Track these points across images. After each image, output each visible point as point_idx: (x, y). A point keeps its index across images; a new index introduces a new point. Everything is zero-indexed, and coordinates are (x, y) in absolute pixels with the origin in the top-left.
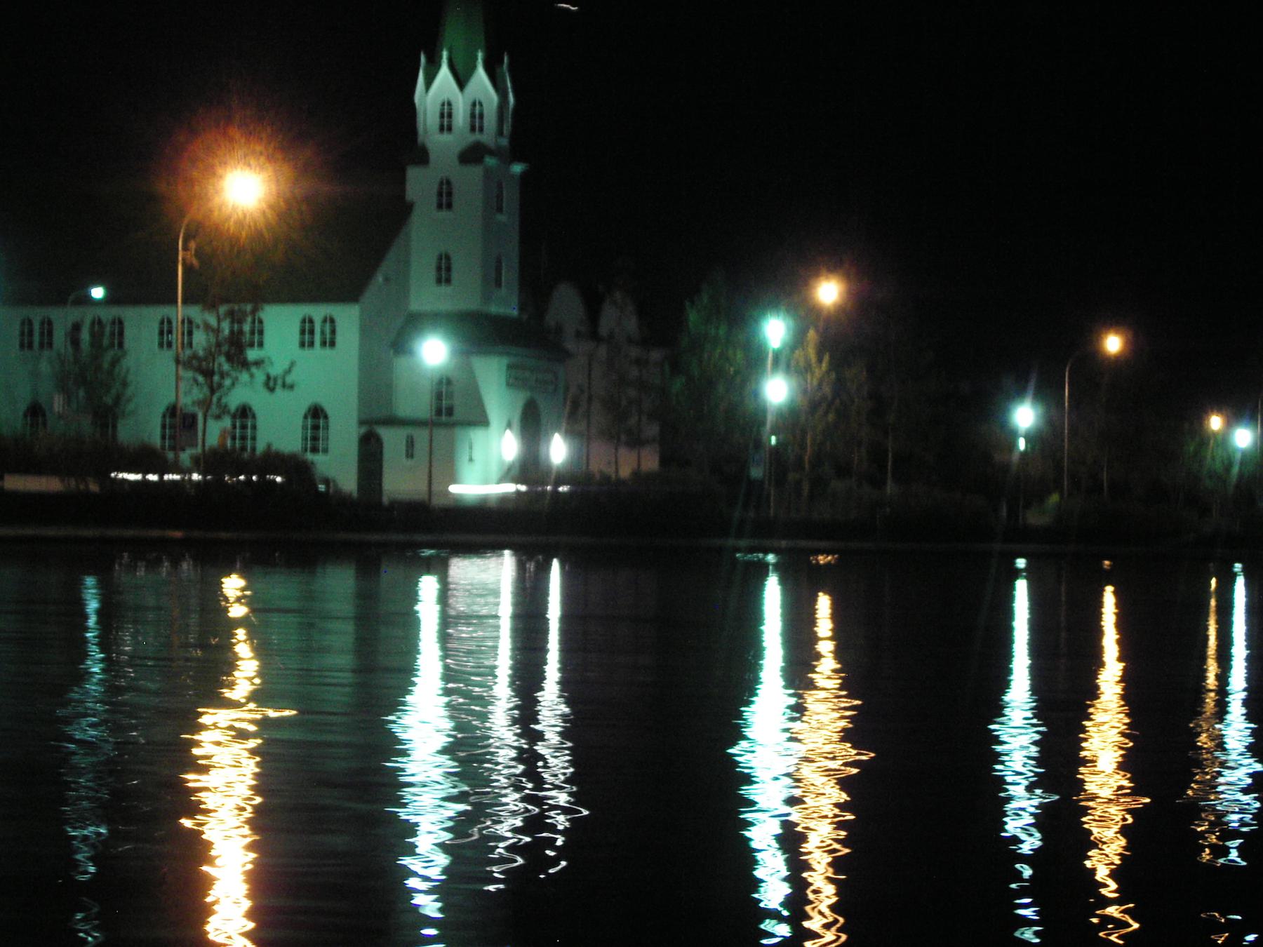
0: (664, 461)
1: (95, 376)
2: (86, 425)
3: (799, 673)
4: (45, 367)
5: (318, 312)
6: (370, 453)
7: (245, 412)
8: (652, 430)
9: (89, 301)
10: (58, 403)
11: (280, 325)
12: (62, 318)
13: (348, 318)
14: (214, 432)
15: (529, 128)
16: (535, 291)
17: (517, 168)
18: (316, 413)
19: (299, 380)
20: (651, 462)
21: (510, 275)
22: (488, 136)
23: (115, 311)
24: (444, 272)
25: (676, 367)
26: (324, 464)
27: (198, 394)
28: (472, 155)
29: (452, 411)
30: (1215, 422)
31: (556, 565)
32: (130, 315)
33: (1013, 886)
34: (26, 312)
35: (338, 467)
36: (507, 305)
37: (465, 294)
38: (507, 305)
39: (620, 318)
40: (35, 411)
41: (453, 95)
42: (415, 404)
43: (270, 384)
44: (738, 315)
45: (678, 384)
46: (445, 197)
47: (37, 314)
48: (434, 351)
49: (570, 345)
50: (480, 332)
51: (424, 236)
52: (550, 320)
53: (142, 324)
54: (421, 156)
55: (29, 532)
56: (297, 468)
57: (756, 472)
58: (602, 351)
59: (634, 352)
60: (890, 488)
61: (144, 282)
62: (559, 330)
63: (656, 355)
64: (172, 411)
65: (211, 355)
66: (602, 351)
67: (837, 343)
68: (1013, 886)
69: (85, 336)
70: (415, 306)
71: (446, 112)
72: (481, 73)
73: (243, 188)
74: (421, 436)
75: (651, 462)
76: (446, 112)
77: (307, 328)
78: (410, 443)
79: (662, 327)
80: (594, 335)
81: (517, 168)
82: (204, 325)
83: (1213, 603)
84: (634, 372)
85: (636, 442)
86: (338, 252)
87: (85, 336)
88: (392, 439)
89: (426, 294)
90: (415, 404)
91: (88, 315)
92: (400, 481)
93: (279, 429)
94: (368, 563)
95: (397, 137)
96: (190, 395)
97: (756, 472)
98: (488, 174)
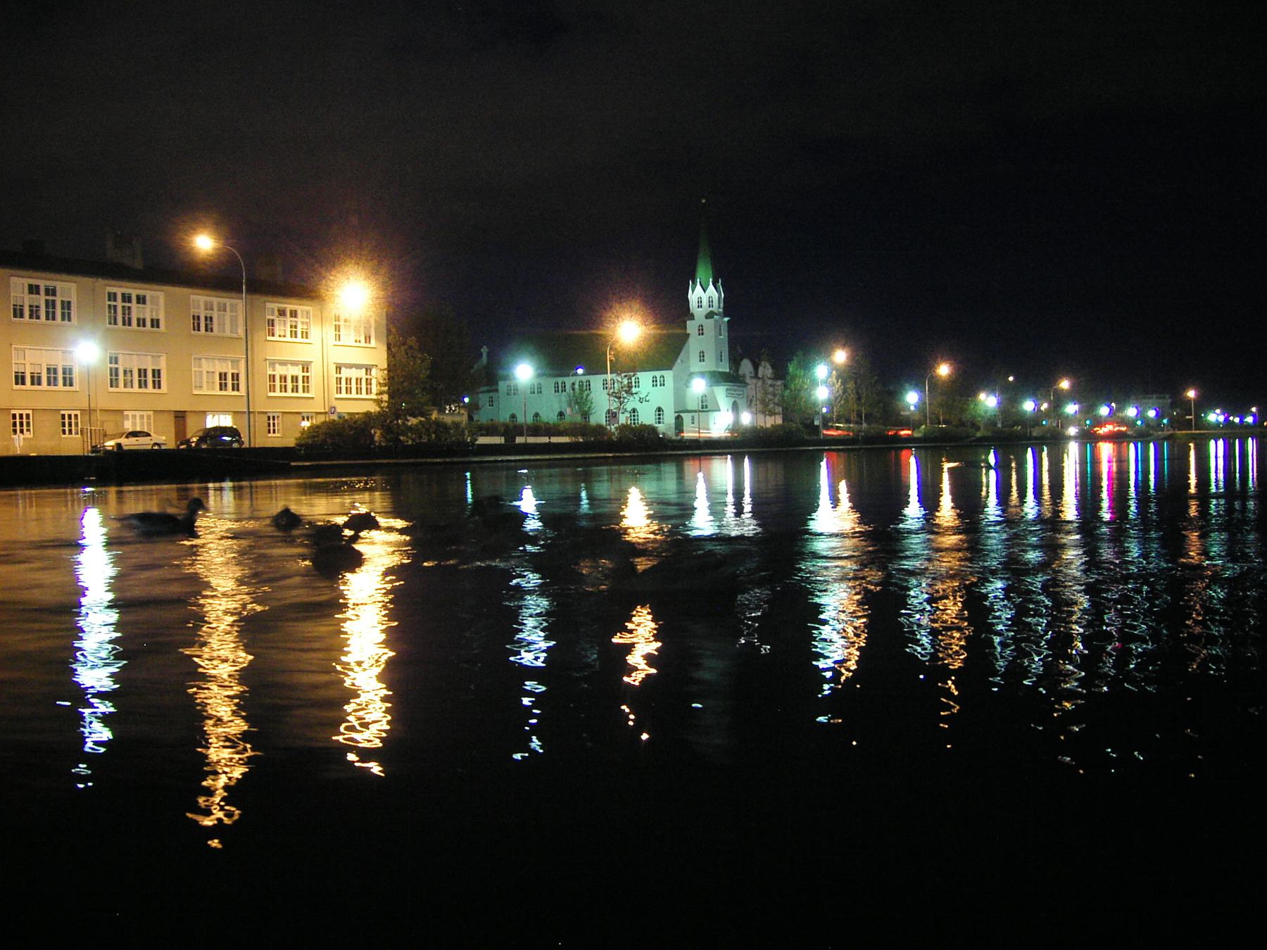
0: (784, 420)
1: (581, 400)
2: (578, 419)
3: (835, 501)
4: (564, 399)
5: (658, 374)
6: (679, 420)
7: (634, 410)
8: (779, 409)
9: (576, 374)
10: (568, 410)
11: (645, 378)
12: (568, 381)
13: (668, 375)
14: (623, 419)
15: (730, 306)
16: (735, 361)
17: (726, 319)
18: (659, 409)
19: (651, 401)
20: (779, 421)
21: (726, 355)
22: (715, 309)
23: (588, 377)
24: (702, 357)
25: (786, 386)
26: (661, 428)
27: (616, 405)
28: (710, 315)
29: (706, 407)
30: (841, 356)
31: (746, 460)
32: (592, 378)
33: (518, 756)
34: (554, 380)
35: (666, 427)
36: (725, 368)
37: (710, 365)
38: (725, 368)
39: (766, 370)
40: (561, 414)
41: (704, 296)
42: (693, 404)
43: (641, 401)
44: (806, 366)
45: (787, 393)
46: (701, 331)
47: (560, 380)
48: (699, 386)
49: (748, 380)
50: (718, 378)
51: (694, 344)
52: (741, 372)
53: (596, 381)
54: (692, 317)
55: (527, 457)
56: (652, 430)
57: (816, 423)
58: (760, 383)
59: (770, 382)
60: (864, 425)
61: (596, 367)
62: (744, 376)
63: (779, 383)
64: (609, 411)
65: (620, 392)
66: (760, 383)
67: (846, 376)
68: (518, 756)
69: (577, 386)
70: (692, 370)
71: (700, 301)
72: (711, 287)
73: (204, 243)
74: (696, 415)
75: (779, 421)
76: (700, 301)
77: (655, 380)
78: (693, 418)
79: (780, 373)
80: (756, 376)
81: (726, 319)
82: (621, 380)
83: (1013, 465)
84: (771, 389)
85: (772, 413)
86: (665, 353)
87: (577, 386)
88: (686, 417)
89: (696, 366)
90: (693, 404)
91: (577, 380)
92: (689, 434)
93: (647, 417)
94: (679, 461)
95: (684, 312)
96: (614, 406)
97: (816, 423)
98: (716, 321)
